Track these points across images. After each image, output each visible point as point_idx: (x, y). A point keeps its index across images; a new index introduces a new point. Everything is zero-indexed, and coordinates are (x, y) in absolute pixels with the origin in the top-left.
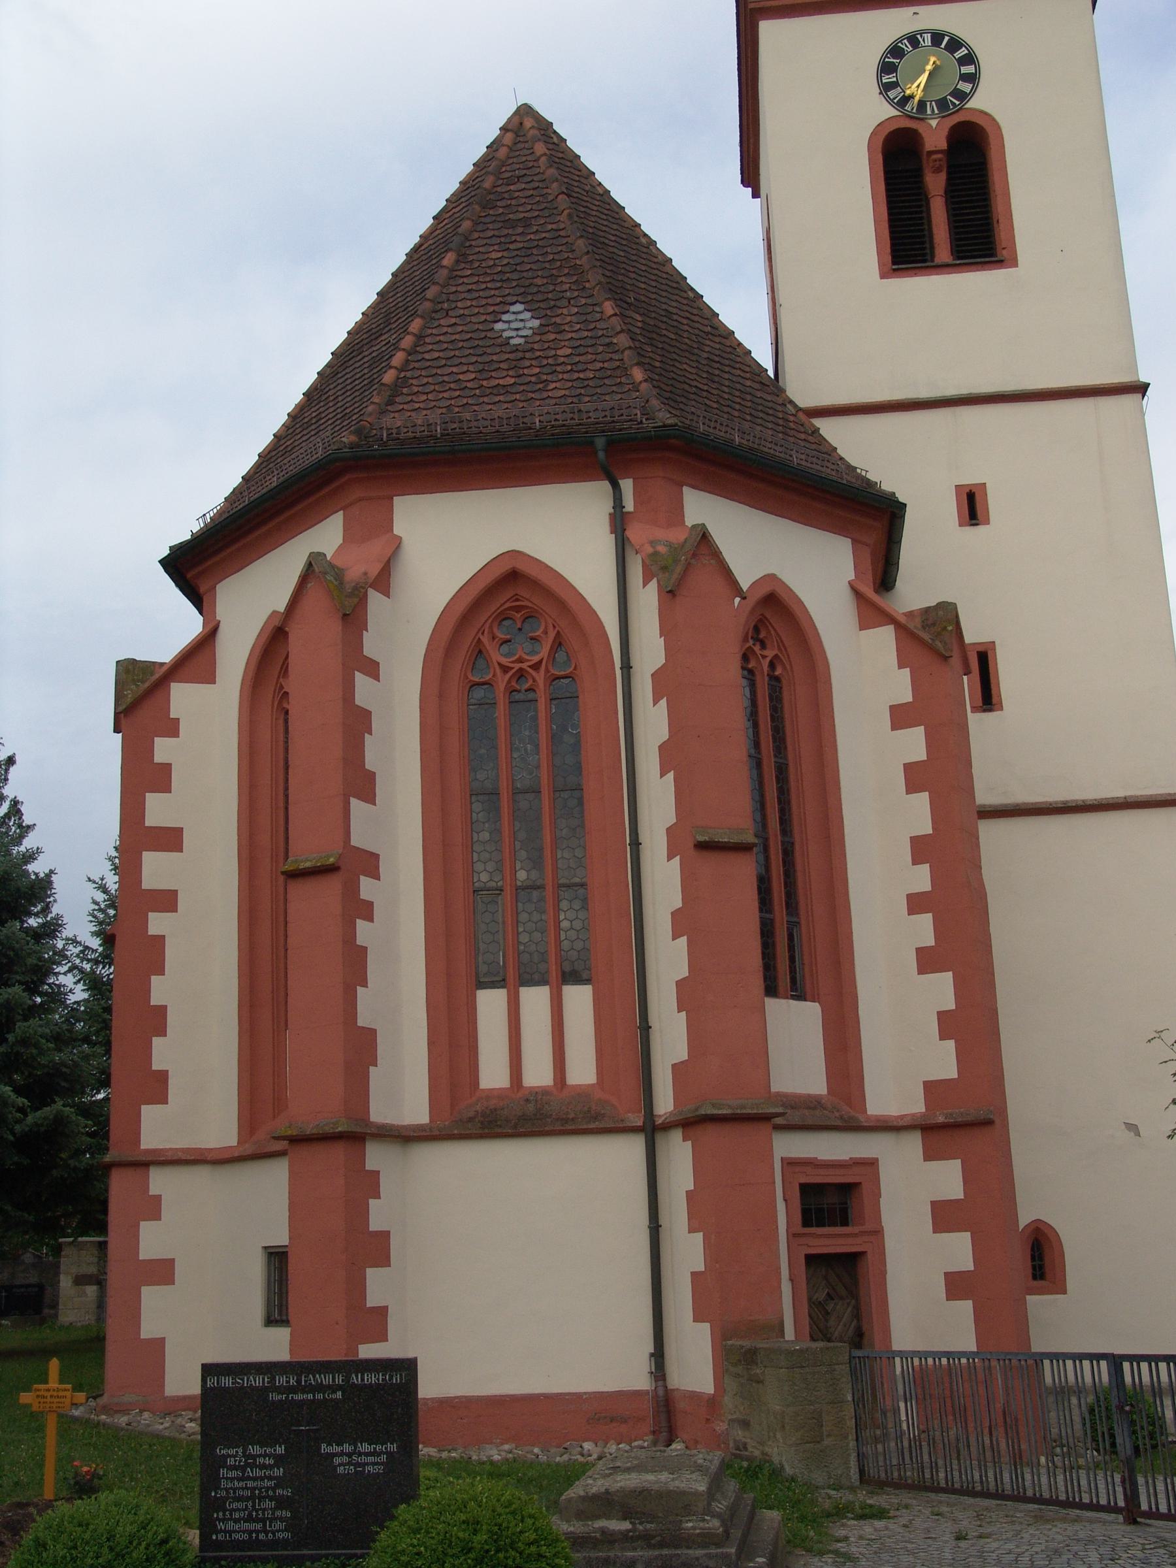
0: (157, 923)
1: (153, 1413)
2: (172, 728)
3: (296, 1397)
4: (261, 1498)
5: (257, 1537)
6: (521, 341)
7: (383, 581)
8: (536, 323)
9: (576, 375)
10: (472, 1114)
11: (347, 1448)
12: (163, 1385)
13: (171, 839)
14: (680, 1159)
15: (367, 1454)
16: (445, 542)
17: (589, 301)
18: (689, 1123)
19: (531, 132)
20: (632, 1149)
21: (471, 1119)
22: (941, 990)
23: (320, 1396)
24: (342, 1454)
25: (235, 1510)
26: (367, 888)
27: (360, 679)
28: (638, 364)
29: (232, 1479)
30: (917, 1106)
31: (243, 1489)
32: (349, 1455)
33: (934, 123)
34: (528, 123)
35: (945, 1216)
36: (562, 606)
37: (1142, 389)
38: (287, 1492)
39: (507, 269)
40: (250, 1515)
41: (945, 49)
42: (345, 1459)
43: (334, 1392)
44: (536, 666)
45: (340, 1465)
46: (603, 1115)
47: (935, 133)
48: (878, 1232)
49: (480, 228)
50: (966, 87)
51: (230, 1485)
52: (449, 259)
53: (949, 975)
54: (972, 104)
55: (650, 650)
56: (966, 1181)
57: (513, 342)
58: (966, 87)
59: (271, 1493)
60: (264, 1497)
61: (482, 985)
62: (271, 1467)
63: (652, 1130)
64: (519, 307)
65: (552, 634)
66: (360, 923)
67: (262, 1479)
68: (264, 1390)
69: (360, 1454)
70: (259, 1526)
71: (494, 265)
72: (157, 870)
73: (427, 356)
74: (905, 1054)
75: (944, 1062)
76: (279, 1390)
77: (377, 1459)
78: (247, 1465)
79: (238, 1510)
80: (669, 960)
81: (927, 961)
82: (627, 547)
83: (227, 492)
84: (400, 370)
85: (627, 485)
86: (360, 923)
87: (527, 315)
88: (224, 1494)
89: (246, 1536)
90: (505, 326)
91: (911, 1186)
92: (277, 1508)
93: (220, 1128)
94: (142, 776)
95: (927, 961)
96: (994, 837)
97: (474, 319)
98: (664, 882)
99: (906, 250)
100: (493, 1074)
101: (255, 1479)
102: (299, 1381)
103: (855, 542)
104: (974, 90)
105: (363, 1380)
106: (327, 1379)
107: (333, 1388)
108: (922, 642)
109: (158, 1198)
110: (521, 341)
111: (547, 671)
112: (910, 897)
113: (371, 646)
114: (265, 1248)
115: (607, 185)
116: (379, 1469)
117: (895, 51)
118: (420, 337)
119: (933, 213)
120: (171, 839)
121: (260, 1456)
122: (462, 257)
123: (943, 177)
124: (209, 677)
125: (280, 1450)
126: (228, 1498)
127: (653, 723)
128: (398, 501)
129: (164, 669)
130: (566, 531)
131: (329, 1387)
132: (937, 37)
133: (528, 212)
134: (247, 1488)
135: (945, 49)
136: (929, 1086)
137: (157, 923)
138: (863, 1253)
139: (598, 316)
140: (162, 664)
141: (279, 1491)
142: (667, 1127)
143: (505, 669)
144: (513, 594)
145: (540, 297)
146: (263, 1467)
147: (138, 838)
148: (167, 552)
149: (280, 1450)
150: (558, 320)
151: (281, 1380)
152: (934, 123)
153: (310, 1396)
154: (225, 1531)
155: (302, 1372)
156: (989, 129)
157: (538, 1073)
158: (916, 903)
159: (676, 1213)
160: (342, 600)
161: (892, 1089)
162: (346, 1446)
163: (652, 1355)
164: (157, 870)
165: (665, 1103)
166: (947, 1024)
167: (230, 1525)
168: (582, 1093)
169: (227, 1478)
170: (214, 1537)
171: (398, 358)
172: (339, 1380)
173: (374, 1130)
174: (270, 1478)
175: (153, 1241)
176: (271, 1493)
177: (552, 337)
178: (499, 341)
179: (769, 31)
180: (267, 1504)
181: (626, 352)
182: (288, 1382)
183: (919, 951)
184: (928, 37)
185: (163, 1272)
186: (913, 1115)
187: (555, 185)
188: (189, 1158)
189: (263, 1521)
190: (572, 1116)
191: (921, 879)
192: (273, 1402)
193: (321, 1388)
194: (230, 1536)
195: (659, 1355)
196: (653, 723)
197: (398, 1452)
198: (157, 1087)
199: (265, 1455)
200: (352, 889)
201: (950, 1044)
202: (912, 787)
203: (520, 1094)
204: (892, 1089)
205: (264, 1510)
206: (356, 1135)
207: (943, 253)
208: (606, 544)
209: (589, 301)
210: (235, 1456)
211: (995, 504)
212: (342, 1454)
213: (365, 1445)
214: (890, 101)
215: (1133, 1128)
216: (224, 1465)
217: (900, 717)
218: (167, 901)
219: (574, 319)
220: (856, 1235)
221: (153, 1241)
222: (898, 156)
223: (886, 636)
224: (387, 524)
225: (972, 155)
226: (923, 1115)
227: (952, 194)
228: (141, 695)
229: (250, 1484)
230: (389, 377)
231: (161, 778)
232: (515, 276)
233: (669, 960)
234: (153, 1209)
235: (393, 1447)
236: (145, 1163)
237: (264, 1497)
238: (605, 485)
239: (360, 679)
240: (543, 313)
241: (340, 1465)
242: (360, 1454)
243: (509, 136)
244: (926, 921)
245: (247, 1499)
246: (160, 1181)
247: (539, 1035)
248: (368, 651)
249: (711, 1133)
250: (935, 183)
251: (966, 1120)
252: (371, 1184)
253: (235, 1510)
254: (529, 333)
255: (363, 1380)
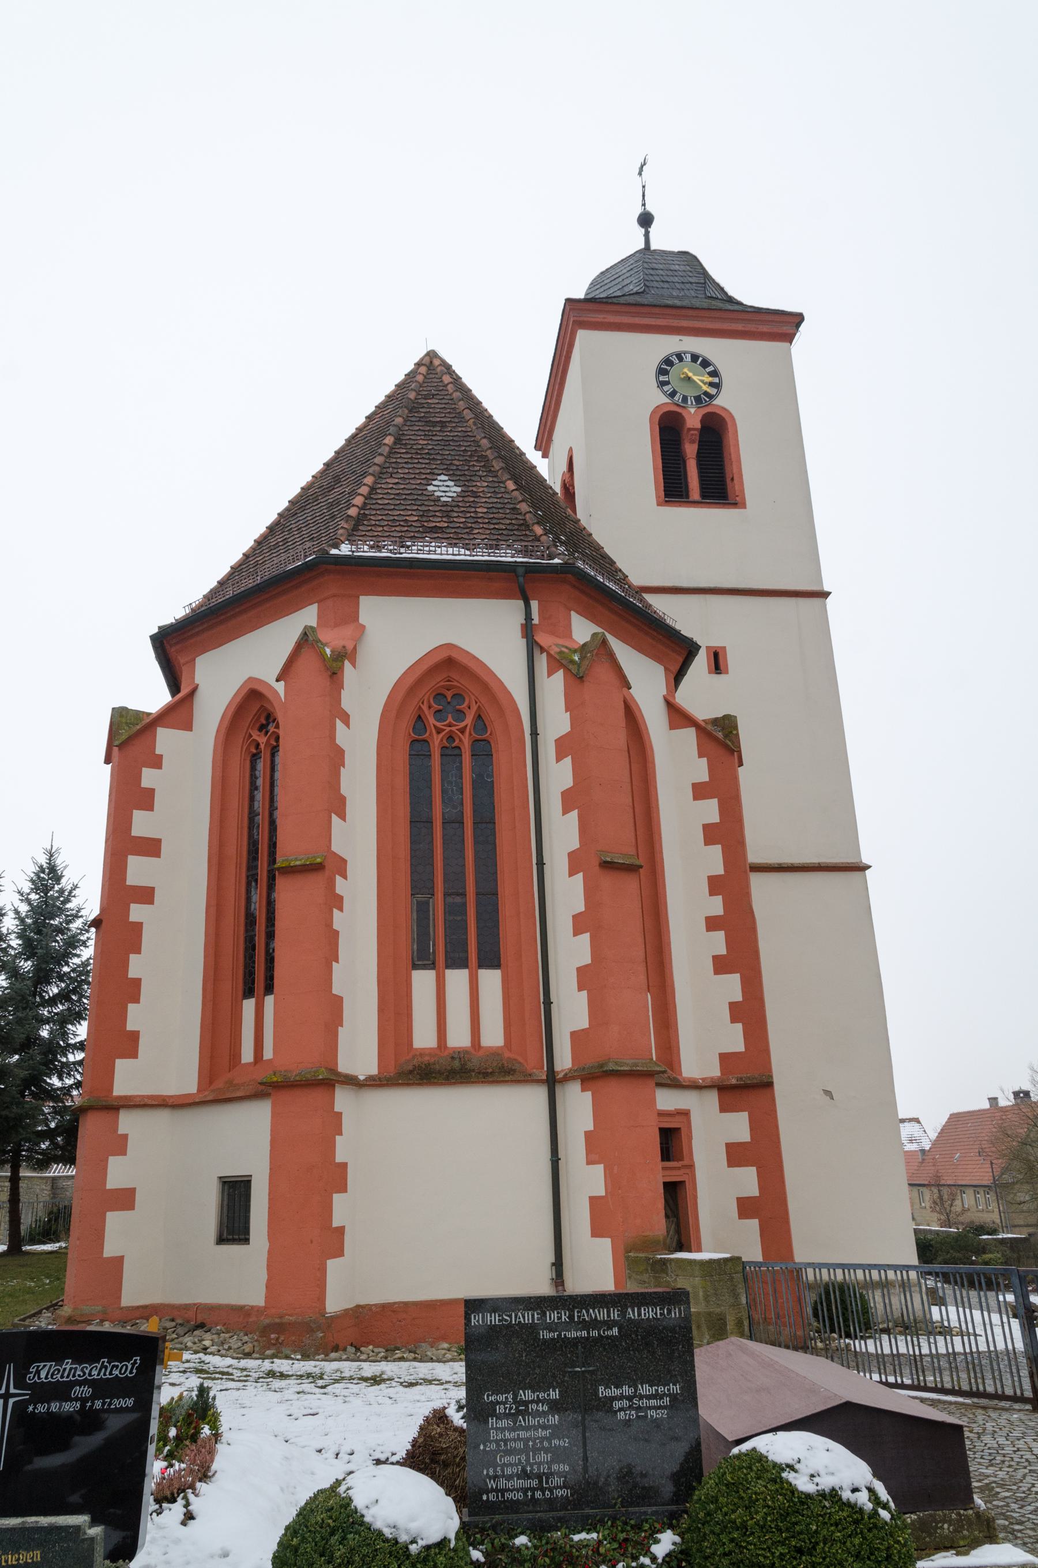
0: (137, 912)
1: (112, 1322)
2: (157, 762)
3: (569, 1335)
4: (536, 1451)
5: (533, 1495)
6: (450, 499)
7: (345, 655)
8: (459, 489)
9: (492, 526)
10: (411, 1068)
11: (627, 1390)
12: (120, 1298)
13: (151, 847)
14: (579, 1107)
15: (649, 1397)
16: (396, 636)
17: (495, 479)
18: (592, 1075)
19: (439, 368)
20: (535, 1097)
21: (411, 1072)
22: (732, 986)
23: (594, 1333)
24: (621, 1397)
25: (507, 1465)
26: (341, 886)
27: (339, 724)
28: (538, 523)
29: (503, 1430)
30: (715, 1071)
31: (515, 1440)
32: (630, 1398)
33: (692, 410)
34: (437, 362)
35: (736, 1155)
36: (485, 687)
37: (826, 595)
38: (565, 1443)
39: (432, 452)
40: (524, 1470)
41: (700, 364)
42: (625, 1403)
43: (610, 1328)
44: (462, 731)
45: (620, 1410)
46: (514, 1071)
47: (693, 417)
48: (691, 1167)
49: (408, 423)
50: (713, 391)
51: (500, 1437)
52: (389, 440)
53: (737, 977)
54: (717, 402)
55: (556, 721)
56: (752, 1129)
57: (443, 499)
58: (713, 391)
59: (546, 1444)
60: (539, 1450)
61: (415, 967)
62: (544, 1414)
63: (552, 1082)
64: (443, 477)
65: (474, 708)
66: (335, 911)
67: (535, 1428)
68: (532, 1328)
69: (641, 1397)
70: (534, 1483)
71: (422, 448)
72: (139, 871)
73: (379, 502)
74: (705, 1037)
75: (733, 1039)
76: (550, 1328)
77: (659, 1403)
78: (519, 1412)
79: (511, 1465)
80: (570, 952)
81: (721, 966)
82: (536, 651)
83: (206, 591)
84: (361, 509)
85: (534, 605)
86: (335, 911)
87: (451, 483)
88: (494, 1446)
89: (520, 1496)
90: (436, 489)
91: (715, 1131)
92: (552, 1461)
93: (184, 1079)
94: (128, 797)
95: (721, 966)
96: (758, 883)
97: (412, 482)
98: (567, 894)
99: (673, 490)
100: (424, 1037)
101: (527, 1428)
102: (571, 1317)
103: (666, 669)
104: (718, 393)
105: (639, 1314)
106: (601, 1315)
107: (609, 1324)
108: (716, 739)
109: (125, 1137)
110: (450, 499)
111: (470, 734)
112: (708, 919)
113: (347, 701)
114: (220, 1178)
115: (491, 411)
116: (663, 1414)
117: (668, 361)
118: (373, 489)
119: (688, 468)
120: (151, 847)
121: (532, 1401)
122: (398, 441)
123: (696, 446)
124: (187, 725)
125: (554, 1394)
126: (498, 1451)
127: (558, 776)
128: (363, 599)
129: (147, 720)
130: (489, 633)
131: (604, 1322)
132: (695, 358)
133: (431, 412)
134: (519, 1439)
135: (700, 364)
136: (724, 1058)
137: (137, 912)
138: (682, 1183)
139: (503, 490)
140: (149, 714)
141: (555, 1442)
142: (568, 1078)
143: (439, 731)
144: (446, 686)
145: (459, 473)
146: (538, 1414)
147: (122, 844)
148: (156, 630)
149: (554, 1394)
150: (474, 489)
151: (552, 1316)
152: (692, 410)
153: (584, 1333)
154: (497, 1490)
155: (574, 1307)
156: (728, 419)
157: (459, 1038)
158: (712, 924)
159: (574, 1148)
160: (323, 664)
161: (698, 1060)
162: (625, 1388)
163: (553, 1264)
164: (139, 871)
165: (564, 1060)
166: (737, 1012)
167: (502, 1483)
168: (495, 1053)
169: (497, 1429)
170: (485, 1497)
171: (358, 501)
172: (615, 1315)
173: (342, 1079)
174: (544, 1427)
175: (118, 1173)
176: (546, 1444)
177: (472, 499)
178: (432, 498)
179: (584, 338)
180: (543, 1457)
181: (527, 516)
182: (559, 1318)
183: (715, 957)
184: (689, 356)
185: (125, 1199)
186: (712, 1078)
187: (461, 403)
188: (154, 1103)
189: (539, 1477)
190: (490, 1070)
191: (716, 906)
192: (545, 1341)
193: (594, 1324)
194: (503, 1496)
195: (558, 1264)
196: (558, 776)
197: (682, 1394)
198: (129, 1044)
199: (538, 1401)
200: (331, 885)
201: (739, 1026)
202: (709, 841)
203: (446, 1053)
204: (698, 1060)
205: (539, 1464)
206: (329, 1080)
207: (695, 493)
208: (521, 644)
209: (495, 479)
210: (504, 1403)
211: (732, 660)
212: (621, 1397)
213: (646, 1386)
214: (664, 393)
215: (828, 1093)
216: (494, 1414)
217: (700, 792)
218: (146, 895)
219: (486, 490)
220: (679, 1168)
221: (118, 1173)
222: (668, 429)
223: (690, 734)
224: (353, 617)
225: (715, 434)
226: (719, 1078)
227: (701, 458)
228: (130, 739)
229: (523, 1434)
230: (353, 512)
231: (146, 800)
232: (439, 457)
233: (570, 952)
234: (120, 1145)
235: (675, 1389)
236: (114, 1107)
237: (539, 1450)
238: (521, 603)
239: (339, 724)
240: (462, 483)
241: (620, 1410)
242: (641, 1397)
243: (423, 370)
244: (720, 936)
245: (519, 1452)
246: (127, 1122)
247: (464, 1007)
248: (345, 704)
249: (615, 1089)
250: (691, 450)
251: (745, 1084)
252: (335, 1123)
253: (507, 1465)
254: (455, 495)
255: (639, 1314)
